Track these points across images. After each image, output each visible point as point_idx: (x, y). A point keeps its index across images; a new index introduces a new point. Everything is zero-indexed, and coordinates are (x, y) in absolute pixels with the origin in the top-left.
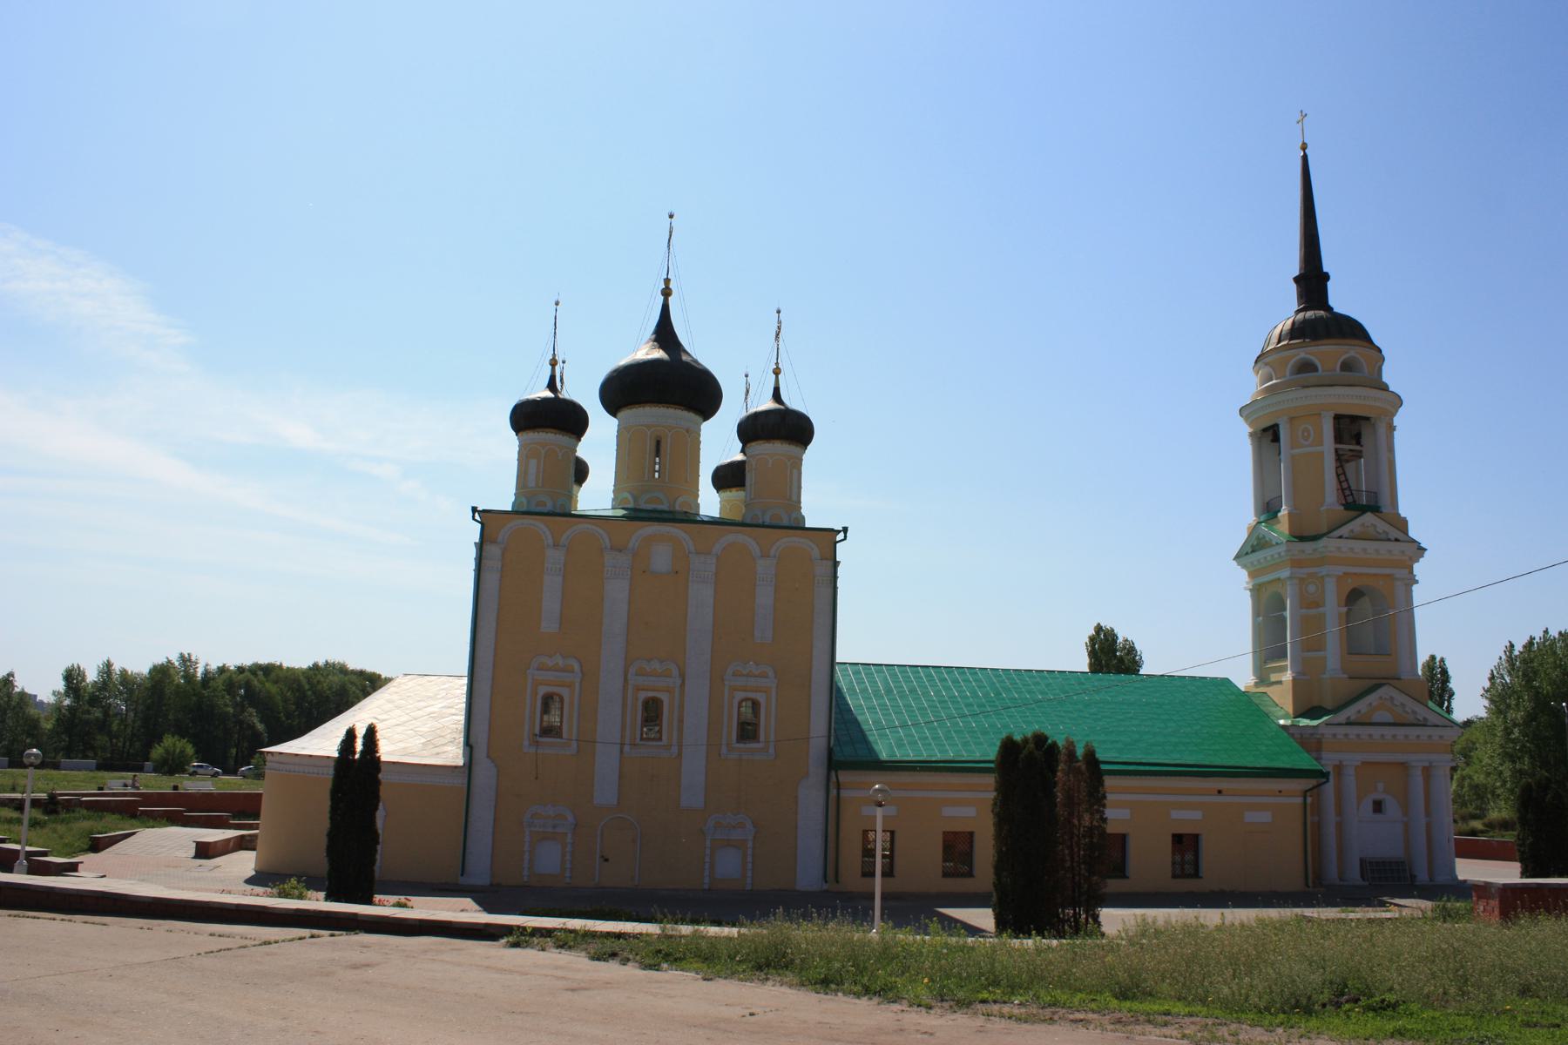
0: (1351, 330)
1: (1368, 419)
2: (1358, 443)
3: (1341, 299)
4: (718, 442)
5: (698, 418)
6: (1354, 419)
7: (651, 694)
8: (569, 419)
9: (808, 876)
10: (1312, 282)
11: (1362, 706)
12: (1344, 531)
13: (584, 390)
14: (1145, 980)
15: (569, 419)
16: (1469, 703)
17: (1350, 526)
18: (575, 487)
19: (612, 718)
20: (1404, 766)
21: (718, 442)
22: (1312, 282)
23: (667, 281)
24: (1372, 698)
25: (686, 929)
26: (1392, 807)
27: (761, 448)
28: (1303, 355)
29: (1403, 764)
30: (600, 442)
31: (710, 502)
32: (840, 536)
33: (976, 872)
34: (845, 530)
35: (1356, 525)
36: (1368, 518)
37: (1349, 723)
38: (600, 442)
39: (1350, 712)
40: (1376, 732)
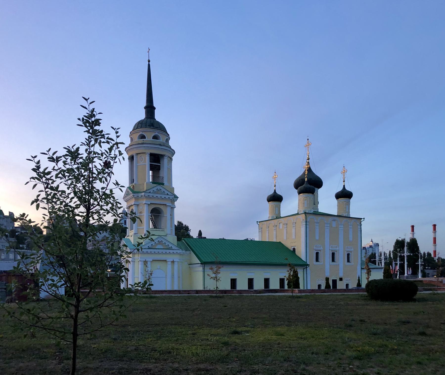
0: (161, 128)
3: (159, 117)
10: (150, 109)
22: (150, 109)
28: (157, 133)
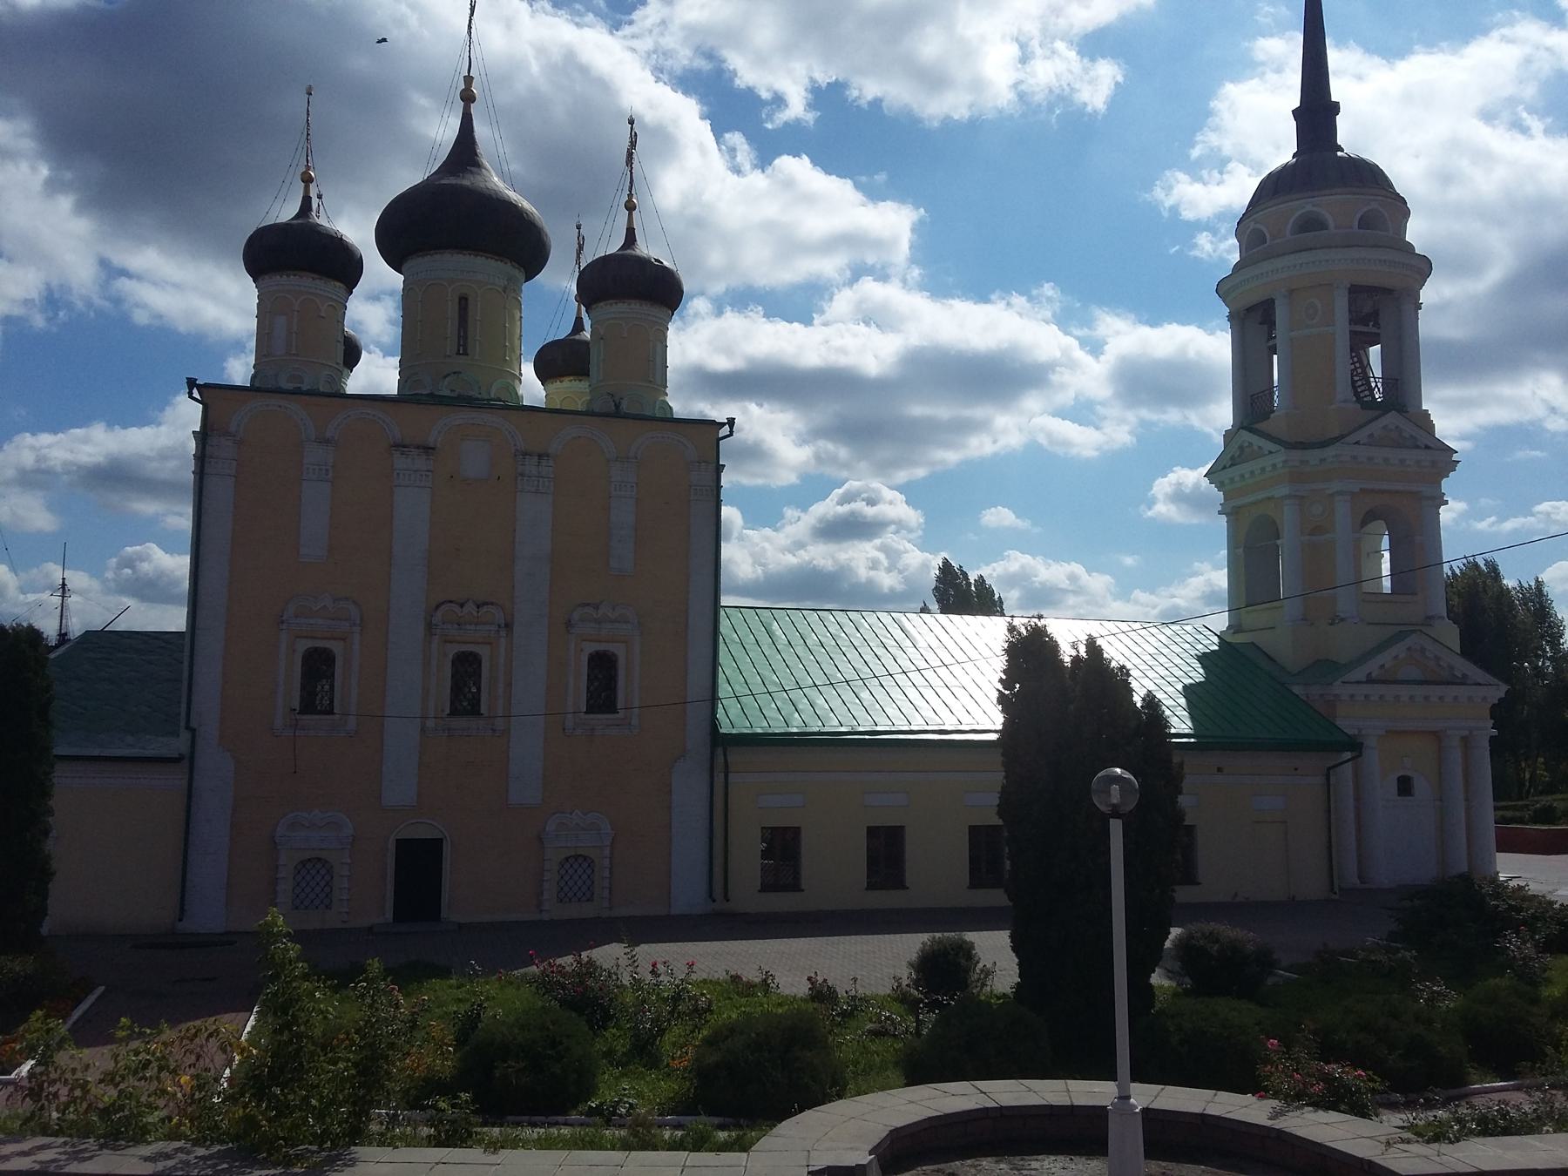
0: (1367, 177)
1: (1388, 291)
2: (1377, 324)
3: (1350, 136)
4: (550, 302)
5: (519, 274)
6: (1372, 290)
7: (465, 648)
8: (341, 266)
9: (688, 894)
11: (1386, 658)
12: (1362, 435)
13: (356, 228)
14: (1549, 981)
15: (341, 266)
16: (1180, 722)
17: (1366, 431)
18: (346, 371)
19: (411, 680)
20: (1437, 736)
21: (550, 302)
23: (469, 80)
24: (1399, 650)
25: (567, 961)
26: (1421, 786)
27: (614, 310)
28: (1309, 208)
29: (1434, 733)
30: (375, 308)
31: (531, 387)
32: (725, 430)
33: (910, 877)
34: (731, 422)
35: (1376, 428)
36: (1391, 419)
37: (1370, 680)
38: (375, 308)
39: (1372, 667)
40: (1404, 692)
